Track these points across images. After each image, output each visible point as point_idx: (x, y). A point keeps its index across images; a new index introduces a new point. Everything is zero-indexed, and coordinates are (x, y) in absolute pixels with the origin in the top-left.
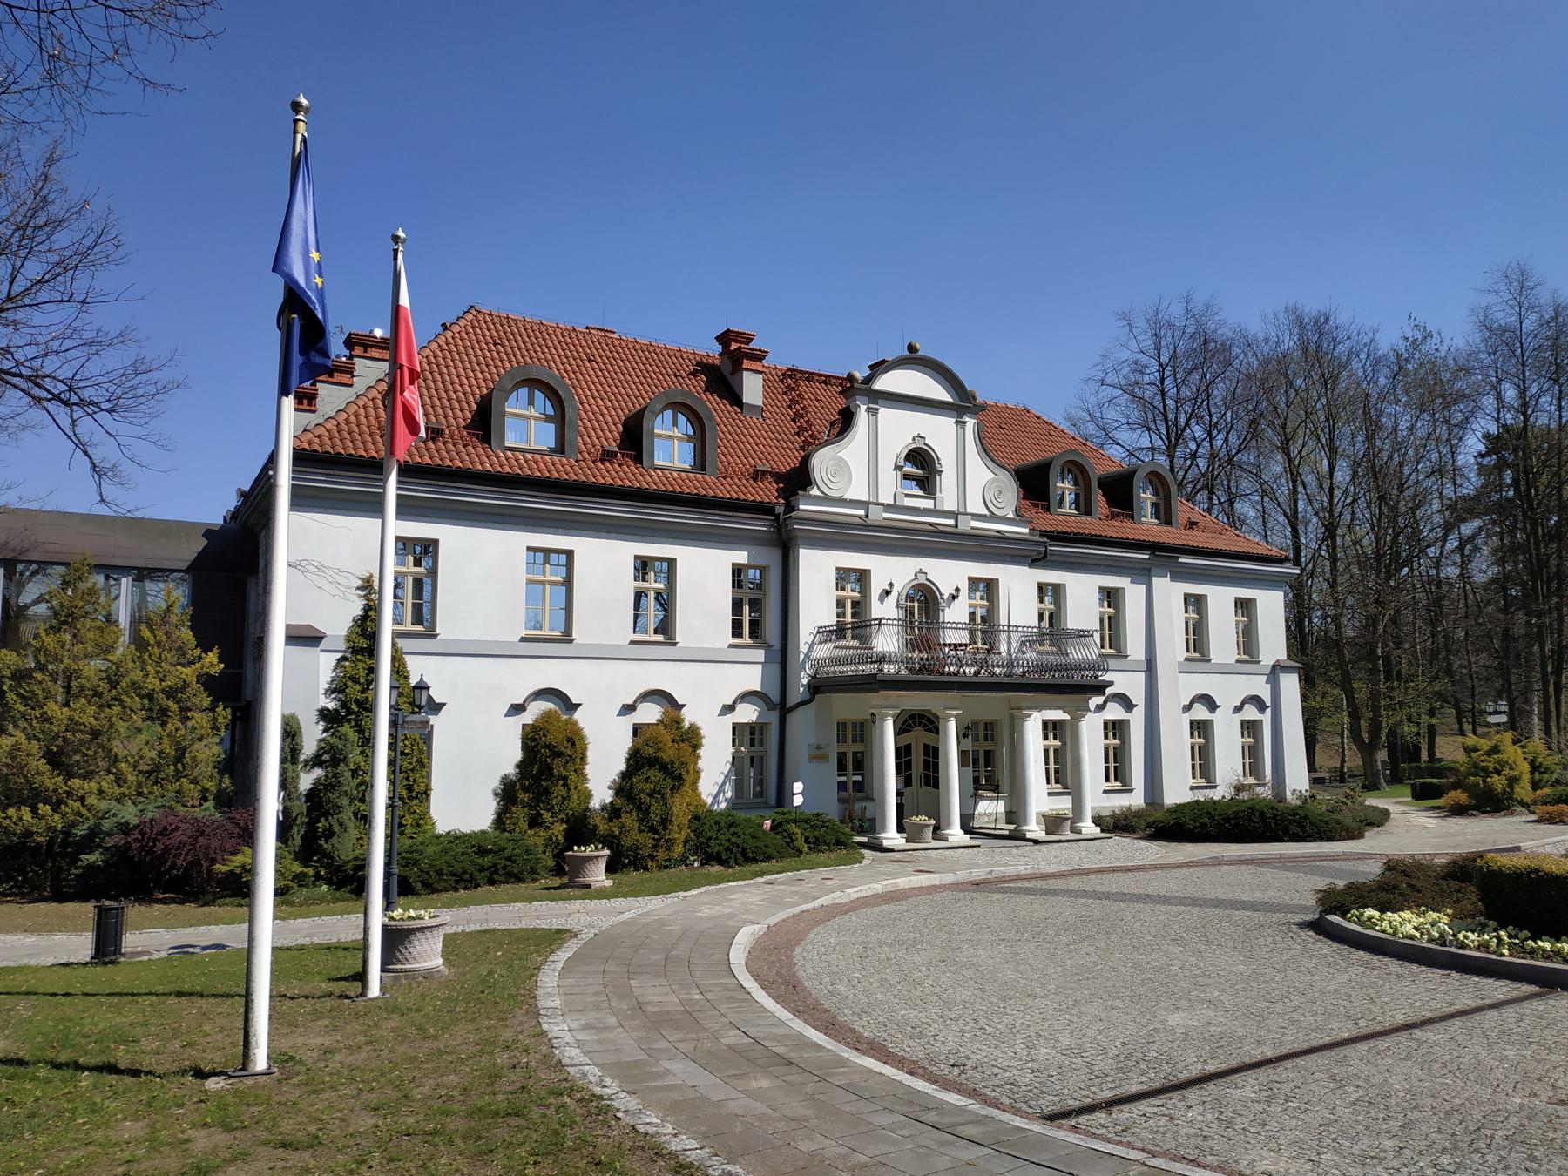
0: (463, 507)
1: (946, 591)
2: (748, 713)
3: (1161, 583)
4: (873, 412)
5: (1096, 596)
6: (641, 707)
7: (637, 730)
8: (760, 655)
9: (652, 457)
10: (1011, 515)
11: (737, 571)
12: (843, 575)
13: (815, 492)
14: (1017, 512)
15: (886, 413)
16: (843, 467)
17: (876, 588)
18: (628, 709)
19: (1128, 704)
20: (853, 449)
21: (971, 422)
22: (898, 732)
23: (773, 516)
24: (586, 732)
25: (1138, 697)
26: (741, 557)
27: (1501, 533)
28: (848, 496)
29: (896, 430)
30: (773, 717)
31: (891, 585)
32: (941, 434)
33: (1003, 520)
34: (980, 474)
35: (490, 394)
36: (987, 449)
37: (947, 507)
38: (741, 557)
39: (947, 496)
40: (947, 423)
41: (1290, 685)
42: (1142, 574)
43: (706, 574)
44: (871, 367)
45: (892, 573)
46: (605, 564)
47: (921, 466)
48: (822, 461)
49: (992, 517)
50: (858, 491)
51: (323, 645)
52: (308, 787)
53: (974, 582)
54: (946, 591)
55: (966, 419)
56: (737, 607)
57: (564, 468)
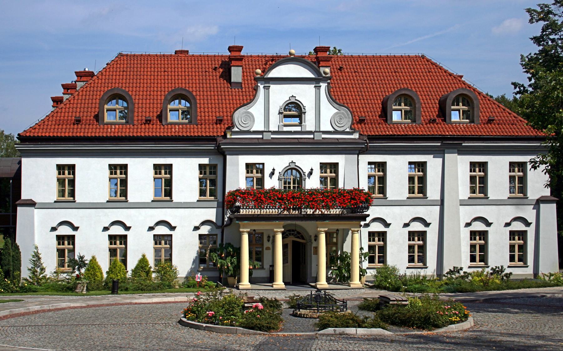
0: (150, 151)
1: (307, 171)
2: (205, 230)
4: (267, 88)
5: (407, 166)
6: (473, 224)
7: (201, 237)
10: (348, 130)
12: (249, 167)
13: (236, 129)
14: (351, 128)
15: (273, 88)
16: (251, 117)
17: (267, 172)
18: (196, 228)
19: (528, 224)
20: (257, 109)
21: (323, 86)
22: (283, 238)
23: (214, 144)
25: (531, 218)
26: (205, 161)
27: (533, 106)
28: (253, 129)
29: (280, 95)
30: (218, 232)
31: (274, 170)
32: (305, 94)
34: (329, 111)
35: (388, 99)
37: (308, 129)
38: (205, 161)
39: (309, 124)
40: (310, 88)
41: (550, 212)
42: (439, 152)
43: (187, 172)
44: (78, 74)
45: (275, 163)
46: (141, 171)
47: (294, 109)
48: (239, 116)
49: (336, 132)
50: (258, 126)
53: (323, 166)
54: (307, 171)
55: (321, 84)
57: (128, 132)
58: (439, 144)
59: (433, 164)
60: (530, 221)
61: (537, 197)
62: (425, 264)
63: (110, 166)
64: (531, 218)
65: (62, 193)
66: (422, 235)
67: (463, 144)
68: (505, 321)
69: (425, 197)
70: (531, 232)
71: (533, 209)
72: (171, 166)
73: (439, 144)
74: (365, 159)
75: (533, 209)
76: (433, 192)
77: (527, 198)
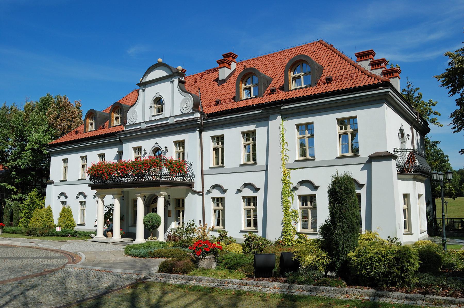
3: (276, 123)
10: (191, 112)
13: (128, 124)
14: (193, 110)
15: (147, 89)
29: (150, 93)
33: (188, 114)
37: (166, 116)
39: (167, 113)
40: (167, 85)
58: (260, 111)
59: (261, 132)
60: (361, 183)
61: (371, 152)
62: (410, 230)
63: (338, 120)
64: (260, 184)
65: (344, 149)
66: (312, 198)
67: (282, 108)
68: (107, 247)
69: (313, 159)
70: (260, 196)
71: (362, 169)
72: (312, 123)
73: (260, 111)
74: (207, 135)
75: (362, 169)
76: (261, 160)
77: (315, 159)
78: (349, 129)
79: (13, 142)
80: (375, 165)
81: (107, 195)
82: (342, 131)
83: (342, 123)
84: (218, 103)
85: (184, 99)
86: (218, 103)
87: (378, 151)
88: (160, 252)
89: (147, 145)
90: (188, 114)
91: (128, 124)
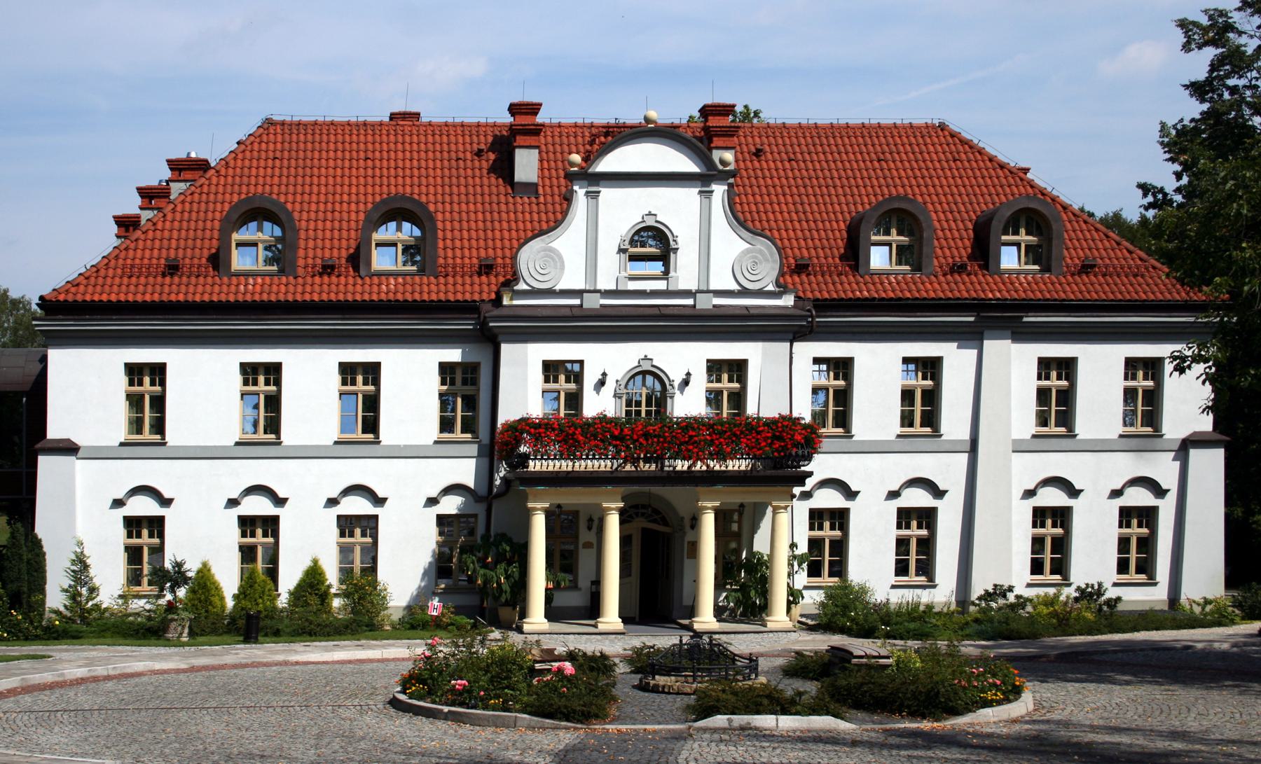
1: (677, 377)
2: (451, 505)
3: (996, 348)
5: (900, 366)
8: (473, 450)
9: (369, 263)
10: (771, 288)
11: (446, 370)
13: (522, 286)
14: (778, 284)
15: (608, 194)
16: (556, 259)
17: (590, 379)
23: (475, 319)
24: (46, 548)
26: (454, 355)
28: (560, 286)
29: (621, 210)
32: (678, 210)
33: (760, 293)
36: (741, 218)
37: (682, 286)
38: (454, 355)
39: (685, 274)
40: (690, 195)
41: (1210, 467)
42: (971, 336)
43: (412, 378)
46: (311, 374)
47: (653, 243)
49: (744, 292)
50: (573, 279)
51: (80, 454)
52: (404, 603)
54: (677, 377)
55: (714, 187)
56: (445, 400)
58: (972, 319)
60: (1164, 487)
61: (1183, 434)
67: (1025, 319)
71: (1174, 459)
73: (972, 319)
78: (147, 386)
79: (480, 266)
80: (1193, 453)
81: (37, 530)
82: (132, 388)
83: (134, 372)
84: (173, 269)
85: (746, 252)
86: (173, 269)
87: (1197, 430)
88: (614, 699)
89: (608, 364)
90: (760, 293)
91: (522, 286)
